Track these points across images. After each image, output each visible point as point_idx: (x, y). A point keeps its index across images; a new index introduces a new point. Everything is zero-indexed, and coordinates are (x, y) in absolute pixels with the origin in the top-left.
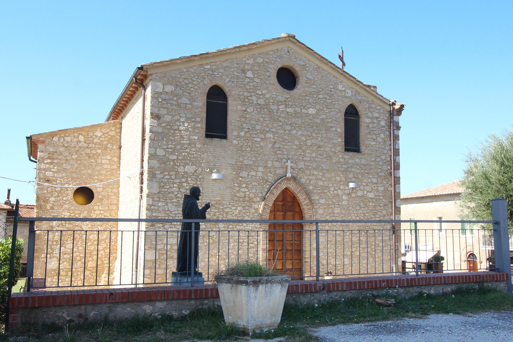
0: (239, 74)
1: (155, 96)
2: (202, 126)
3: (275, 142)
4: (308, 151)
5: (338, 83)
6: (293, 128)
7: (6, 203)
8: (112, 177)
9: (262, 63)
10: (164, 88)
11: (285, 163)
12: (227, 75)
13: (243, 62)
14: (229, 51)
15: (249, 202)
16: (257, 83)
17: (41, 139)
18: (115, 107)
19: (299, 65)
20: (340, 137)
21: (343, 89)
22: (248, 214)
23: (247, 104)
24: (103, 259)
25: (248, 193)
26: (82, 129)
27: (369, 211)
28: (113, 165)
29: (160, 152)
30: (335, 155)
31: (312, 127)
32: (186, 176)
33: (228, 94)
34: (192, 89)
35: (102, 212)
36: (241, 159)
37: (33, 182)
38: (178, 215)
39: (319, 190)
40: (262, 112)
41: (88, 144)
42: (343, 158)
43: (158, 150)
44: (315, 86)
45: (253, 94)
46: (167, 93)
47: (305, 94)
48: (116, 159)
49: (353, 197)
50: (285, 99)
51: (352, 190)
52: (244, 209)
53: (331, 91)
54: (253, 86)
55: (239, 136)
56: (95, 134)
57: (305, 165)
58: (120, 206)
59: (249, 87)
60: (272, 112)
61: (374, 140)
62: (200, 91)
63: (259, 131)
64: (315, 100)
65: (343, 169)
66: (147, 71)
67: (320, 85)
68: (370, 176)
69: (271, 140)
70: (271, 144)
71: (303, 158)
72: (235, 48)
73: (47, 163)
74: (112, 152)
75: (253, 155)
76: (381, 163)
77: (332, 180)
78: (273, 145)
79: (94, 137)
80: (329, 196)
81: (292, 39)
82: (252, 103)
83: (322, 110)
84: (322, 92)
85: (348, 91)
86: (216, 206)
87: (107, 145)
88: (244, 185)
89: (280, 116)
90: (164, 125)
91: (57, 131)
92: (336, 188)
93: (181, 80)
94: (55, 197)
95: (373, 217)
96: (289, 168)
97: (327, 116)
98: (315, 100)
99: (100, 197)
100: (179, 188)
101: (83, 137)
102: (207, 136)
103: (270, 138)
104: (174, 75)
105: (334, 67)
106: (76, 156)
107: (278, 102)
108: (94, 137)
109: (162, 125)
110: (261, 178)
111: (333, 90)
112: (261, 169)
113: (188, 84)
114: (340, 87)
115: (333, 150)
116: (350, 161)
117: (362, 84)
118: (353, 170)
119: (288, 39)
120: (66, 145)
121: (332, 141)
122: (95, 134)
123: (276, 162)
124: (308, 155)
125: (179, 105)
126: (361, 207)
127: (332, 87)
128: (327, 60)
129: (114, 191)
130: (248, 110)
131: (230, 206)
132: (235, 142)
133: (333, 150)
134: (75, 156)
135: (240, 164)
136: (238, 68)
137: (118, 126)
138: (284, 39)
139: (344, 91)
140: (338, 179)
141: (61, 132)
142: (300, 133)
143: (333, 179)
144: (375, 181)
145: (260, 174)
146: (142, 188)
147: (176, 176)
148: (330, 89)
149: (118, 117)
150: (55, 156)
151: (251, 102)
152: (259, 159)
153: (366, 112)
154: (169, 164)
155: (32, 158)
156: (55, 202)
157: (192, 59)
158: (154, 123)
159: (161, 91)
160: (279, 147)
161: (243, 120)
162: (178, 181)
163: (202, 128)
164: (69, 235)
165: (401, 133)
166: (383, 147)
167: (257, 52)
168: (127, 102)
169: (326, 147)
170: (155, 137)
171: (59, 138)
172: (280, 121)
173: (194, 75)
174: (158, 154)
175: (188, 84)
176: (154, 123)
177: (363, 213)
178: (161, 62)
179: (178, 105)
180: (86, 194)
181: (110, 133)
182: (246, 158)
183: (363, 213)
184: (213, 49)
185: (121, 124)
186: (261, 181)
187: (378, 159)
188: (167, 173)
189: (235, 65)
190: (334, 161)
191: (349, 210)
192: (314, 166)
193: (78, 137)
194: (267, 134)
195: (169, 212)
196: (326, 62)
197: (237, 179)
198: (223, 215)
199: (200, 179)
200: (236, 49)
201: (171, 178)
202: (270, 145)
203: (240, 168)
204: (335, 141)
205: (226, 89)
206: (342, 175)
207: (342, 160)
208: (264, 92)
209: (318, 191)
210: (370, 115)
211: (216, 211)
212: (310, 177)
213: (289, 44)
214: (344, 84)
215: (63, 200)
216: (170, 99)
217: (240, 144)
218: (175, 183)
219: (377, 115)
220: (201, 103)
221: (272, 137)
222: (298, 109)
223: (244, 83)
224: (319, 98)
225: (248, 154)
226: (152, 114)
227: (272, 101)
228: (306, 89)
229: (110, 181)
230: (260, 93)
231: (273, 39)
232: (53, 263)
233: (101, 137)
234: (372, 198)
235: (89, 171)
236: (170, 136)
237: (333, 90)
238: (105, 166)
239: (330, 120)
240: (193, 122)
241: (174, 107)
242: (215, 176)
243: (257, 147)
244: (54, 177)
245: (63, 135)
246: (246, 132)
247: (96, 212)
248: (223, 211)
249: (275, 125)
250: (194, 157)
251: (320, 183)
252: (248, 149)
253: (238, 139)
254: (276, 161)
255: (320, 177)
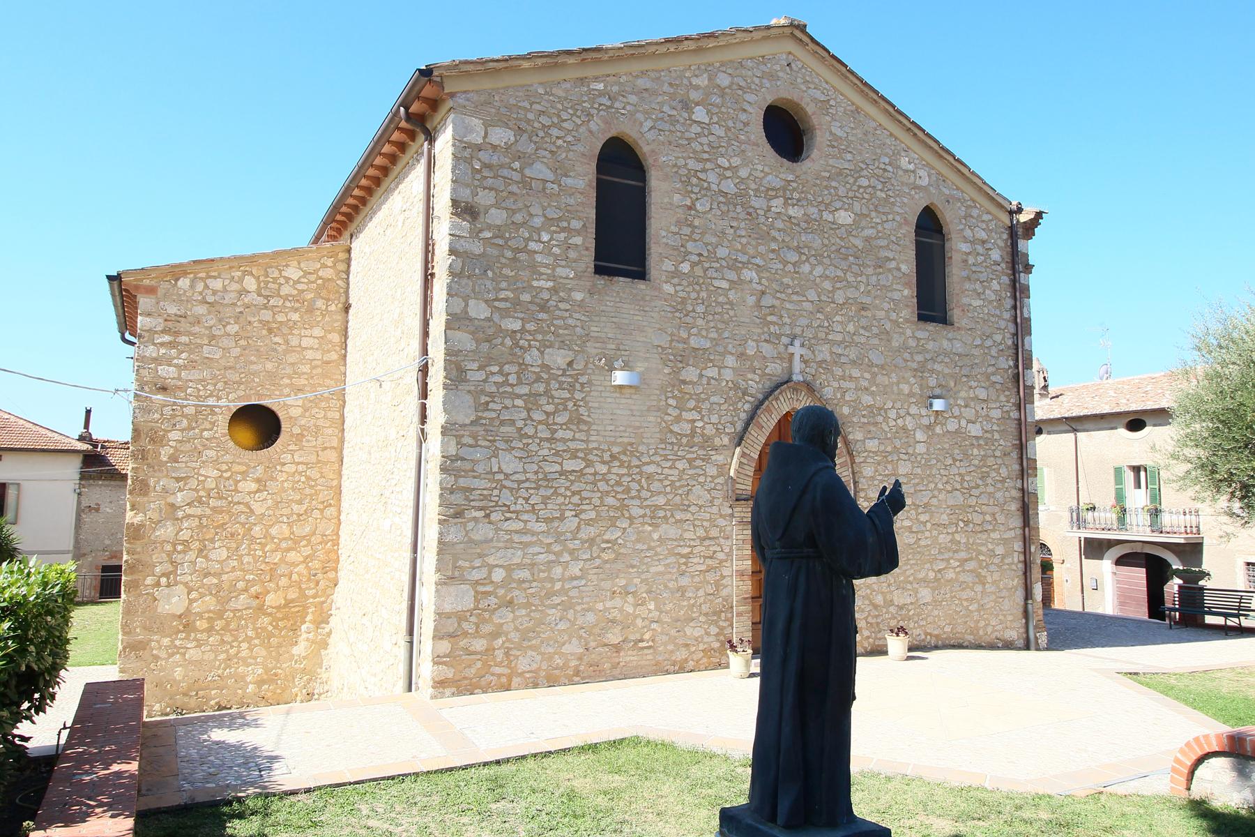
0: (674, 113)
1: (464, 153)
2: (584, 242)
3: (763, 293)
4: (838, 318)
5: (899, 153)
6: (804, 258)
7: (81, 438)
8: (328, 382)
9: (729, 87)
10: (486, 134)
11: (786, 346)
12: (646, 112)
13: (685, 82)
14: (652, 49)
15: (702, 448)
16: (719, 137)
17: (147, 282)
18: (335, 208)
19: (814, 100)
20: (907, 284)
21: (911, 167)
22: (701, 479)
23: (696, 190)
24: (304, 586)
25: (700, 424)
26: (252, 259)
27: (972, 468)
28: (329, 351)
29: (479, 310)
30: (898, 330)
31: (846, 259)
32: (545, 376)
33: (649, 162)
34: (560, 142)
35: (300, 468)
36: (684, 335)
37: (126, 391)
38: (527, 485)
39: (864, 416)
40: (731, 214)
41: (266, 297)
42: (914, 337)
43: (472, 302)
44: (849, 156)
45: (709, 165)
46: (494, 147)
47: (827, 175)
48: (336, 338)
49: (938, 435)
50: (783, 183)
51: (936, 418)
52: (692, 467)
53: (885, 170)
54: (709, 145)
55: (676, 273)
56: (284, 273)
57: (832, 353)
58: (345, 452)
59: (699, 148)
60: (754, 215)
61: (979, 294)
62: (580, 148)
63: (724, 263)
64: (850, 190)
65: (915, 365)
66: (441, 85)
67: (860, 154)
68: (973, 384)
69: (755, 285)
70: (754, 298)
71: (827, 334)
72: (668, 41)
73: (162, 344)
74: (327, 318)
75: (712, 324)
76: (994, 352)
77: (893, 392)
78: (759, 300)
79: (282, 281)
80: (886, 433)
81: (798, 33)
82: (708, 189)
83: (867, 216)
84: (865, 173)
85: (922, 173)
86: (625, 459)
87: (313, 301)
88: (692, 404)
89: (772, 226)
90: (488, 234)
91: (189, 263)
92: (902, 412)
93: (531, 116)
94: (182, 430)
95: (980, 482)
96: (797, 358)
97: (878, 232)
98: (850, 190)
99: (296, 430)
100: (529, 410)
101: (253, 281)
102: (599, 271)
103: (751, 281)
104: (512, 101)
105: (891, 109)
106: (236, 327)
107: (768, 189)
108: (282, 281)
109: (481, 235)
110: (730, 384)
111: (890, 168)
112: (730, 361)
113: (549, 127)
114: (904, 162)
115: (893, 316)
116: (930, 345)
117: (954, 156)
118: (936, 366)
119: (788, 31)
120: (210, 299)
121: (889, 295)
122: (284, 273)
123: (765, 344)
124: (839, 328)
125: (525, 183)
126: (955, 460)
127: (887, 160)
128: (877, 92)
129: (330, 415)
130: (698, 207)
131: (658, 459)
132: (668, 288)
133: (893, 316)
134: (233, 328)
135: (681, 346)
136: (672, 97)
137: (342, 256)
138: (780, 31)
139: (913, 172)
140: (905, 388)
141: (198, 267)
142: (818, 271)
143: (895, 388)
144: (982, 394)
145: (728, 375)
146: (424, 408)
147: (518, 378)
148: (882, 166)
149: (340, 234)
150: (184, 326)
151: (706, 185)
152: (726, 334)
153: (962, 227)
154: (502, 344)
155: (128, 336)
156: (180, 441)
157: (560, 60)
158: (461, 228)
159: (480, 141)
160: (773, 306)
161: (687, 230)
162: (524, 390)
163: (587, 249)
164: (217, 527)
165: (1034, 281)
166: (998, 312)
167: (716, 58)
168: (369, 191)
169: (876, 307)
170: (463, 268)
171: (192, 281)
172: (774, 239)
173: (566, 104)
174: (472, 314)
175: (549, 127)
176: (461, 228)
177: (960, 474)
178: (481, 62)
179: (522, 182)
180: (261, 424)
181: (320, 273)
182: (694, 331)
183: (960, 474)
184: (612, 40)
185: (349, 251)
186: (732, 393)
187: (989, 343)
188: (495, 369)
189: (666, 88)
190: (895, 344)
191: (931, 467)
192: (853, 356)
193: (241, 280)
194: (744, 271)
195: (501, 477)
196: (875, 97)
197: (673, 386)
198: (639, 482)
199: (582, 385)
200: (668, 45)
201: (506, 383)
202: (751, 300)
203: (682, 357)
204: (896, 295)
205: (645, 149)
206: (912, 380)
207: (912, 343)
208: (736, 161)
209: (863, 420)
210: (968, 233)
211: (624, 471)
212: (845, 385)
213: (791, 46)
214: (913, 155)
215: (201, 437)
216: (502, 166)
217: (682, 294)
218: (519, 396)
219: (983, 235)
220: (582, 180)
221: (756, 279)
222: (813, 211)
223: (687, 135)
224: (860, 187)
225: (700, 322)
226: (455, 203)
227: (753, 186)
228: (831, 162)
229: (321, 390)
230: (727, 165)
231: (757, 29)
232: (175, 600)
233: (298, 282)
234: (977, 438)
235: (269, 366)
236: (505, 265)
237: (890, 168)
238: (310, 354)
239: (883, 243)
240: (563, 230)
241: (514, 188)
242: (620, 378)
243: (721, 304)
244: (179, 378)
245: (203, 275)
246: (693, 265)
247: (286, 468)
248: (641, 473)
249: (762, 249)
250: (567, 327)
251: (867, 399)
252: (700, 309)
253: (676, 281)
254: (766, 341)
255: (866, 384)
